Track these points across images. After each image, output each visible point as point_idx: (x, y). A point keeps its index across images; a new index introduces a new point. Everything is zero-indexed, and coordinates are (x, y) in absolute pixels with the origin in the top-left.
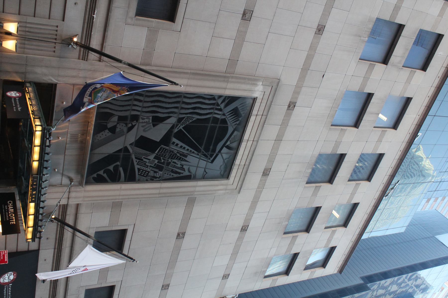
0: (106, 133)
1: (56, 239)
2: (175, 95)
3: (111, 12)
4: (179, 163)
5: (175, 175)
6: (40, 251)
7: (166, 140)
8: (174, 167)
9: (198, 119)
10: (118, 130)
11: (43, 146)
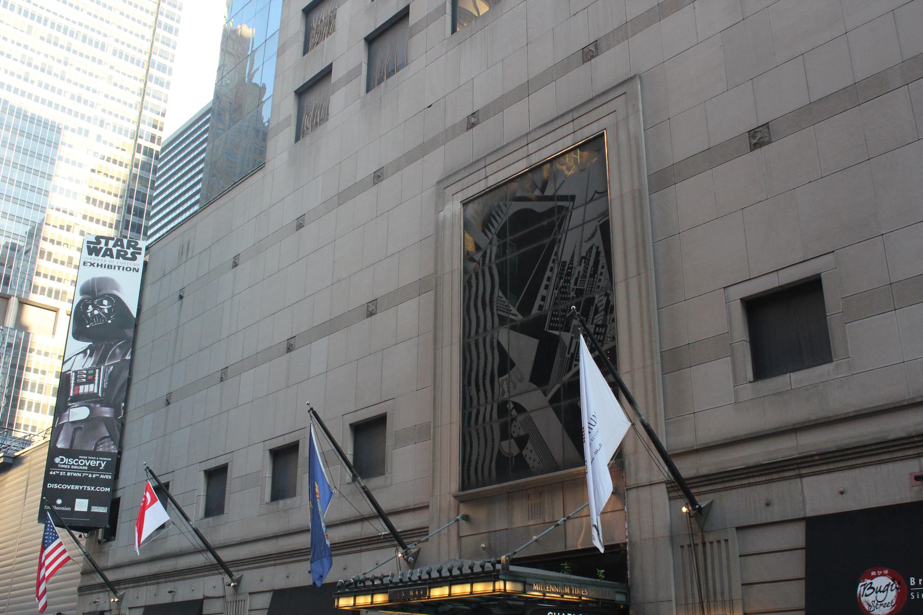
0: (530, 454)
1: (768, 482)
2: (468, 354)
3: (829, 417)
4: (578, 269)
5: (603, 260)
6: (810, 513)
7: (532, 328)
8: (584, 276)
9: (500, 288)
10: (522, 433)
11: (471, 578)
